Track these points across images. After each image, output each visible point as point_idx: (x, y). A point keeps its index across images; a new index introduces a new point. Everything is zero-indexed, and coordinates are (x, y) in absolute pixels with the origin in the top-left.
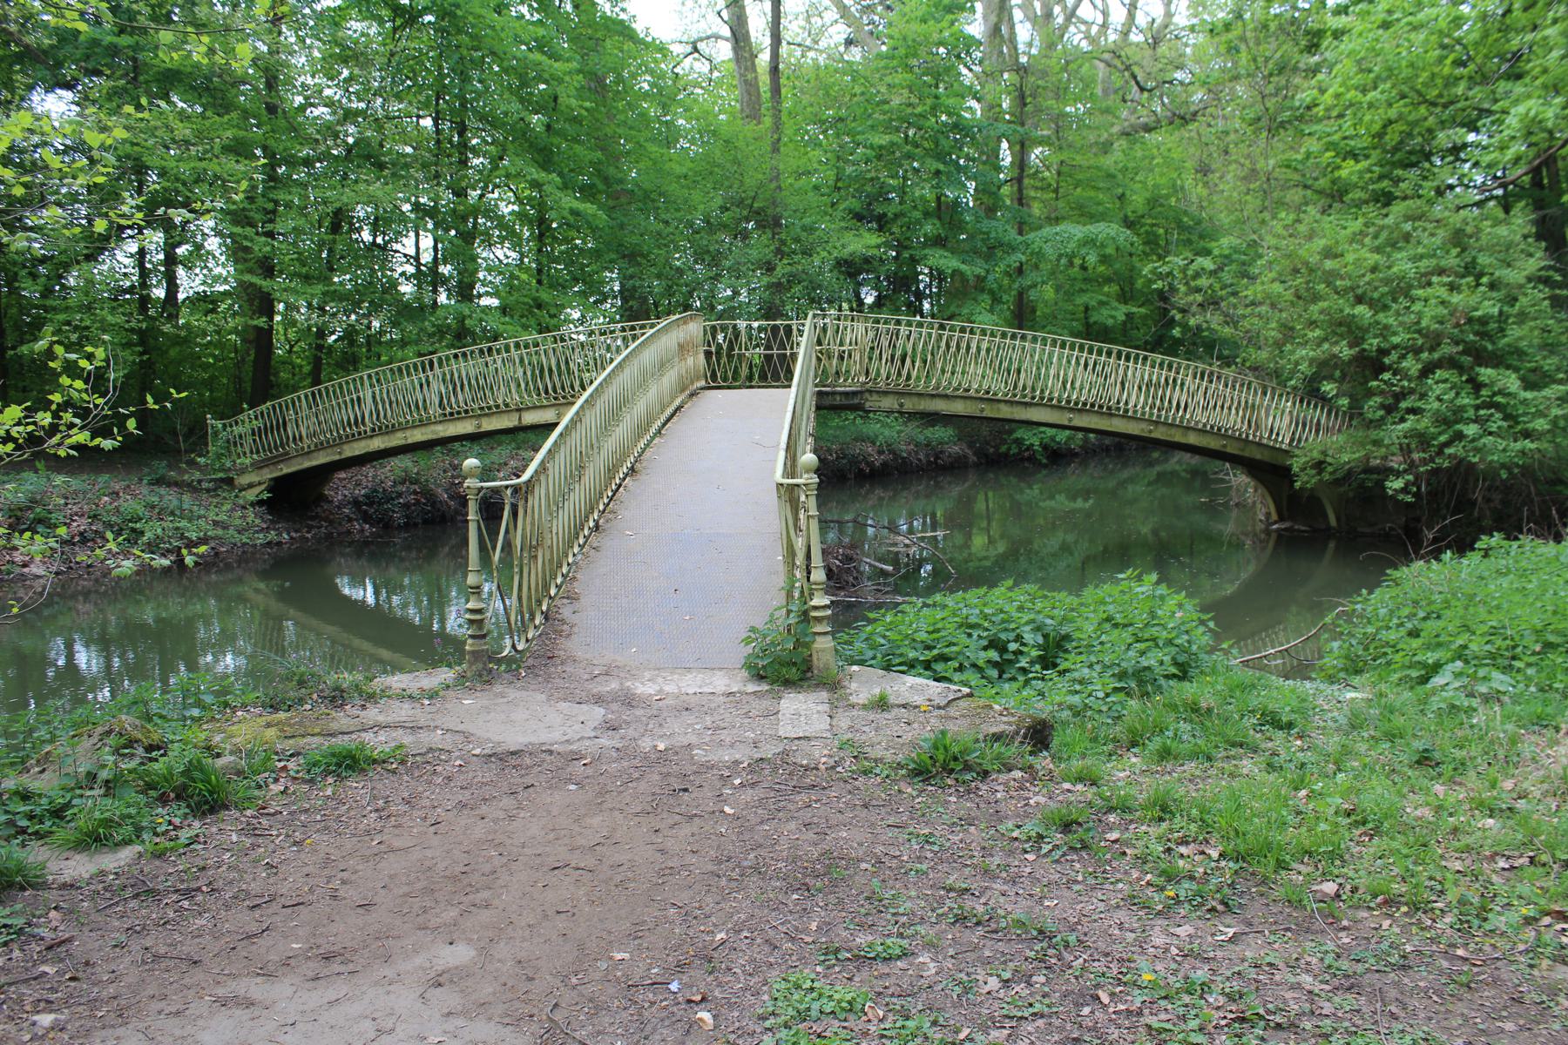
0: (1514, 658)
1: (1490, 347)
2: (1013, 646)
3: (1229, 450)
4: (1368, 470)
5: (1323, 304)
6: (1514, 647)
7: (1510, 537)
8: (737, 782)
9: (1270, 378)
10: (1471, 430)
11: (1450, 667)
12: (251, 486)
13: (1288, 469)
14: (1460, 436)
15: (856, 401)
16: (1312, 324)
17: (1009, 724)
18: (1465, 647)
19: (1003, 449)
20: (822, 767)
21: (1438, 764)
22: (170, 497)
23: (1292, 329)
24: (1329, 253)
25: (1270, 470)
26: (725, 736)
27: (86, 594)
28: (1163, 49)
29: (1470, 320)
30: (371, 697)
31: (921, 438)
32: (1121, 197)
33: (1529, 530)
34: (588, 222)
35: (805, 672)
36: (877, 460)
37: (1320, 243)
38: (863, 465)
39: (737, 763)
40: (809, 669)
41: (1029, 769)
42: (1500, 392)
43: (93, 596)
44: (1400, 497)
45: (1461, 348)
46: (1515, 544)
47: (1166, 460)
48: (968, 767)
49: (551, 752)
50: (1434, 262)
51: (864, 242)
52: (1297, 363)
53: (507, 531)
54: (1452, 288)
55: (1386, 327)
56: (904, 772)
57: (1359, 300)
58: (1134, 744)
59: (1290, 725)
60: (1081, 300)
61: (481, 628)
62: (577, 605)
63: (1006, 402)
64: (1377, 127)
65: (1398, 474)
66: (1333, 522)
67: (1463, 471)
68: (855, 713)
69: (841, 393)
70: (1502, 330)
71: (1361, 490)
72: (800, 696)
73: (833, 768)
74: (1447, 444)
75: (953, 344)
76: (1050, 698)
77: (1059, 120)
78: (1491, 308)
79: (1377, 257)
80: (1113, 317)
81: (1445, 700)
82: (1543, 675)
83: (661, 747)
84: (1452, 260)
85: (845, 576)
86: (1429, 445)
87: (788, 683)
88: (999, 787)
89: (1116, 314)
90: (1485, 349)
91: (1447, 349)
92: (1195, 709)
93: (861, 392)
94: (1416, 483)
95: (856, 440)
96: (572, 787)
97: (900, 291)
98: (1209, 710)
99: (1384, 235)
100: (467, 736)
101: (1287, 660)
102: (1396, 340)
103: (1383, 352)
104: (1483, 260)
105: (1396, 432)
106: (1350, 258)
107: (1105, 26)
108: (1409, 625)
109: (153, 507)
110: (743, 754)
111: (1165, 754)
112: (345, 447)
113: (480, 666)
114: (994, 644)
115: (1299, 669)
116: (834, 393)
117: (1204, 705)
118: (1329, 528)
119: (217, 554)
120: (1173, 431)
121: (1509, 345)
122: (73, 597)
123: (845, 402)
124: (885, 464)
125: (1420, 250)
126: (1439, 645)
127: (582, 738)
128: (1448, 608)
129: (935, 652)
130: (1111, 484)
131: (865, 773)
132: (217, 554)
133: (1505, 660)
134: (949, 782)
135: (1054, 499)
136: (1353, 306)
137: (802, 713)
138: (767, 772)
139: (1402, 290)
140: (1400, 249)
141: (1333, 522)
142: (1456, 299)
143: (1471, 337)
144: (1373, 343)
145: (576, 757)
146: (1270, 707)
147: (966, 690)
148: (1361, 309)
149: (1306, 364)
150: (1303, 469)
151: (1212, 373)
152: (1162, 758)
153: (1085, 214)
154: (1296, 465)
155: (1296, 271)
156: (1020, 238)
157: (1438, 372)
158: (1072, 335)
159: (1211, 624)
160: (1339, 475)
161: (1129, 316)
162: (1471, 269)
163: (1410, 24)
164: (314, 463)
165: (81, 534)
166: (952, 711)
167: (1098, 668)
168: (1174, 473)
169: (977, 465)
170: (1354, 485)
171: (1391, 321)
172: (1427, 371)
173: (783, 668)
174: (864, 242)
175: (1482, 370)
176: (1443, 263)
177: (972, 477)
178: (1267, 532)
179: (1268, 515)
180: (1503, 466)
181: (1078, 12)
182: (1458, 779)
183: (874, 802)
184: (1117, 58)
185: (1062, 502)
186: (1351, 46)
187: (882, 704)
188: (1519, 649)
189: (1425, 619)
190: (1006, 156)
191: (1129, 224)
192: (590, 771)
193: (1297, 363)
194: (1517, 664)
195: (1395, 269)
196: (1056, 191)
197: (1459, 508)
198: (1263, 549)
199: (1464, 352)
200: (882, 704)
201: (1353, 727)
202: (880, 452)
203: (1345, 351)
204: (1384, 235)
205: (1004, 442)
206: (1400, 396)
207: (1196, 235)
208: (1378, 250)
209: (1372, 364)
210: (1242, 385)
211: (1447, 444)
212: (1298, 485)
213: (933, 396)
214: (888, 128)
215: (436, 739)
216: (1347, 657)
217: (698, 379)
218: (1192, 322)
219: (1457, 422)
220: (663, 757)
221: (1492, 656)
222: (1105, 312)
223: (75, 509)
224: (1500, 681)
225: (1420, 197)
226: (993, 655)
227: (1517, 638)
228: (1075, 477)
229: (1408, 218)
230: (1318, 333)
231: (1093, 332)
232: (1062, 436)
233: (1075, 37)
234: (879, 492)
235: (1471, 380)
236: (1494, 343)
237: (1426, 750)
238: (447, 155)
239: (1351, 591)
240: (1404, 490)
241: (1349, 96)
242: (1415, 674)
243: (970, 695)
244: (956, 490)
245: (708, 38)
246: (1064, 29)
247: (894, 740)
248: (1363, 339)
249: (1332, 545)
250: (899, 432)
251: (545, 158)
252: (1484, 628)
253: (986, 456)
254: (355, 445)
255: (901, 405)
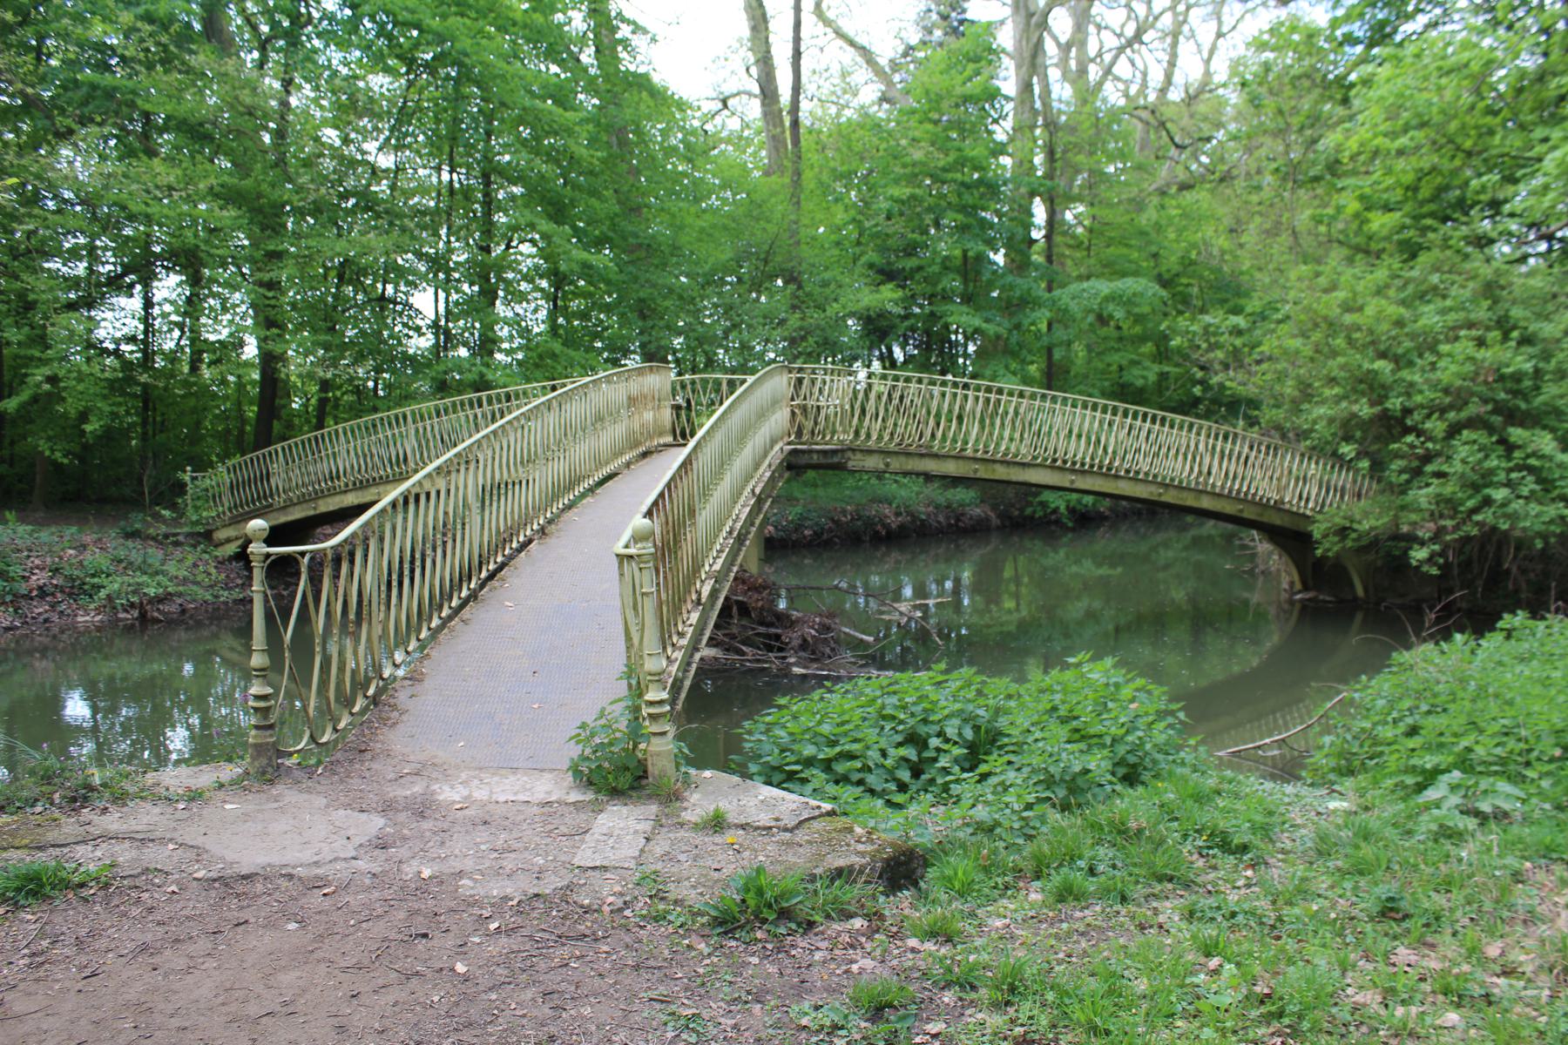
0: (1528, 764)
1: (1523, 406)
2: (934, 742)
3: (1246, 515)
4: (1396, 537)
5: (1341, 360)
6: (1530, 751)
7: (1536, 615)
8: (493, 926)
9: (1287, 436)
10: (1499, 494)
11: (1445, 778)
12: (228, 540)
13: (1309, 535)
14: (1487, 501)
15: (835, 460)
16: (1332, 381)
17: (862, 854)
18: (1469, 750)
19: (1029, 511)
20: (606, 909)
21: (1406, 916)
22: (134, 551)
23: (1310, 385)
24: (1348, 308)
25: (1291, 536)
26: (509, 863)
27: (44, 651)
28: (1201, 108)
29: (1502, 378)
30: (120, 799)
31: (941, 500)
32: (1155, 256)
33: (1557, 611)
34: (600, 275)
35: (640, 778)
36: (894, 522)
37: (1341, 295)
38: (879, 527)
39: (506, 898)
40: (645, 775)
41: (876, 917)
42: (1534, 454)
43: (49, 654)
44: (1425, 568)
45: (1490, 407)
46: (1541, 625)
47: (1201, 525)
48: (785, 914)
49: (290, 877)
50: (1462, 315)
51: (888, 297)
52: (1315, 422)
53: (328, 604)
54: (1481, 343)
55: (1412, 384)
56: (705, 919)
57: (1383, 355)
58: (1038, 876)
59: (1244, 848)
60: (1116, 358)
61: (266, 717)
62: (418, 688)
63: (1002, 462)
64: (1409, 178)
65: (1422, 543)
66: (1360, 591)
67: (1493, 540)
68: (682, 833)
69: (818, 452)
70: (1537, 388)
71: (1386, 555)
72: (625, 810)
73: (620, 910)
74: (1475, 511)
75: (897, 395)
76: (924, 821)
77: (1097, 176)
78: (1522, 362)
79: (1402, 310)
80: (1144, 377)
81: (1435, 820)
82: (1560, 789)
83: (426, 873)
84: (1481, 313)
85: (821, 647)
86: (1456, 512)
87: (616, 793)
88: (812, 950)
89: (1148, 374)
90: (1518, 408)
91: (1474, 409)
92: (1122, 831)
93: (842, 451)
94: (1442, 554)
95: (873, 501)
96: (292, 926)
97: (935, 353)
98: (1140, 831)
99: (1411, 289)
100: (199, 852)
101: (1286, 750)
102: (1419, 399)
103: (1407, 411)
104: (1517, 313)
105: (1423, 496)
106: (1370, 311)
107: (1144, 85)
108: (1410, 721)
109: (120, 561)
110: (515, 889)
111: (1065, 894)
112: (321, 502)
113: (265, 761)
114: (913, 739)
115: (1287, 770)
116: (811, 451)
117: (1133, 825)
118: (1356, 599)
119: (184, 611)
120: (1185, 494)
121: (1546, 404)
122: (30, 652)
123: (823, 461)
124: (902, 527)
125: (1448, 303)
126: (1441, 745)
127: (336, 859)
128: (1454, 701)
129: (838, 749)
130: (1143, 548)
131: (656, 919)
132: (184, 611)
133: (1511, 769)
134: (759, 934)
135: (1077, 565)
136: (1373, 361)
137: (620, 830)
138: (535, 914)
139: (1428, 344)
140: (1429, 302)
141: (1360, 591)
142: (1482, 354)
143: (1502, 395)
144: (1395, 403)
145: (316, 884)
146: (1222, 824)
147: (827, 806)
148: (1380, 364)
149: (1324, 423)
150: (1325, 536)
151: (1236, 435)
152: (1061, 899)
153: (1114, 270)
154: (1317, 531)
155: (1316, 325)
156: (1047, 295)
157: (1465, 432)
158: (1104, 395)
159: (1181, 715)
160: (1364, 542)
161: (1163, 376)
162: (1505, 326)
163: (1439, 68)
164: (290, 518)
165: (40, 588)
166: (801, 836)
167: (1026, 770)
168: (1210, 537)
169: (1000, 529)
170: (1382, 553)
171: (1417, 378)
172: (1454, 431)
173: (617, 776)
174: (888, 297)
175: (1511, 430)
176: (1473, 316)
177: (995, 540)
178: (1291, 602)
179: (1292, 584)
180: (1539, 534)
181: (1115, 70)
182: (1429, 939)
183: (652, 963)
184: (1156, 119)
185: (1088, 568)
186: (1379, 93)
187: (717, 824)
188: (1535, 754)
189: (1429, 712)
190: (1039, 212)
191: (1164, 283)
192: (327, 903)
193: (1315, 422)
194: (1531, 774)
195: (1420, 323)
196: (1088, 249)
197: (1483, 583)
198: (1287, 620)
199: (1495, 411)
200: (717, 824)
201: (1320, 853)
202: (898, 514)
203: (1364, 410)
204: (1411, 289)
205: (1030, 504)
206: (1427, 458)
207: (1228, 293)
208: (1403, 303)
209: (1392, 425)
210: (1268, 447)
211: (1475, 511)
212: (1319, 552)
213: (922, 455)
214: (912, 180)
215: (157, 856)
216: (1340, 755)
217: (661, 434)
218: (1215, 380)
219: (1486, 486)
220: (422, 887)
221: (1503, 761)
222: (1136, 371)
223: (37, 562)
224: (1504, 794)
225: (1450, 247)
226: (910, 753)
227: (1532, 741)
228: (1103, 541)
229: (1436, 269)
230: (1337, 390)
231: (1126, 393)
232: (1089, 499)
233: (1112, 95)
234: (895, 555)
235: (1503, 441)
236: (1527, 401)
237: (1391, 899)
238: (471, 208)
239: (1346, 676)
240: (1430, 560)
241: (1376, 142)
242: (1410, 780)
243: (832, 813)
244: (978, 554)
245: (738, 94)
246: (1100, 84)
247: (706, 872)
248: (1387, 397)
249: (1359, 617)
250: (918, 494)
251: (558, 211)
252: (1495, 727)
253: (1010, 518)
254: (329, 500)
255: (887, 465)
